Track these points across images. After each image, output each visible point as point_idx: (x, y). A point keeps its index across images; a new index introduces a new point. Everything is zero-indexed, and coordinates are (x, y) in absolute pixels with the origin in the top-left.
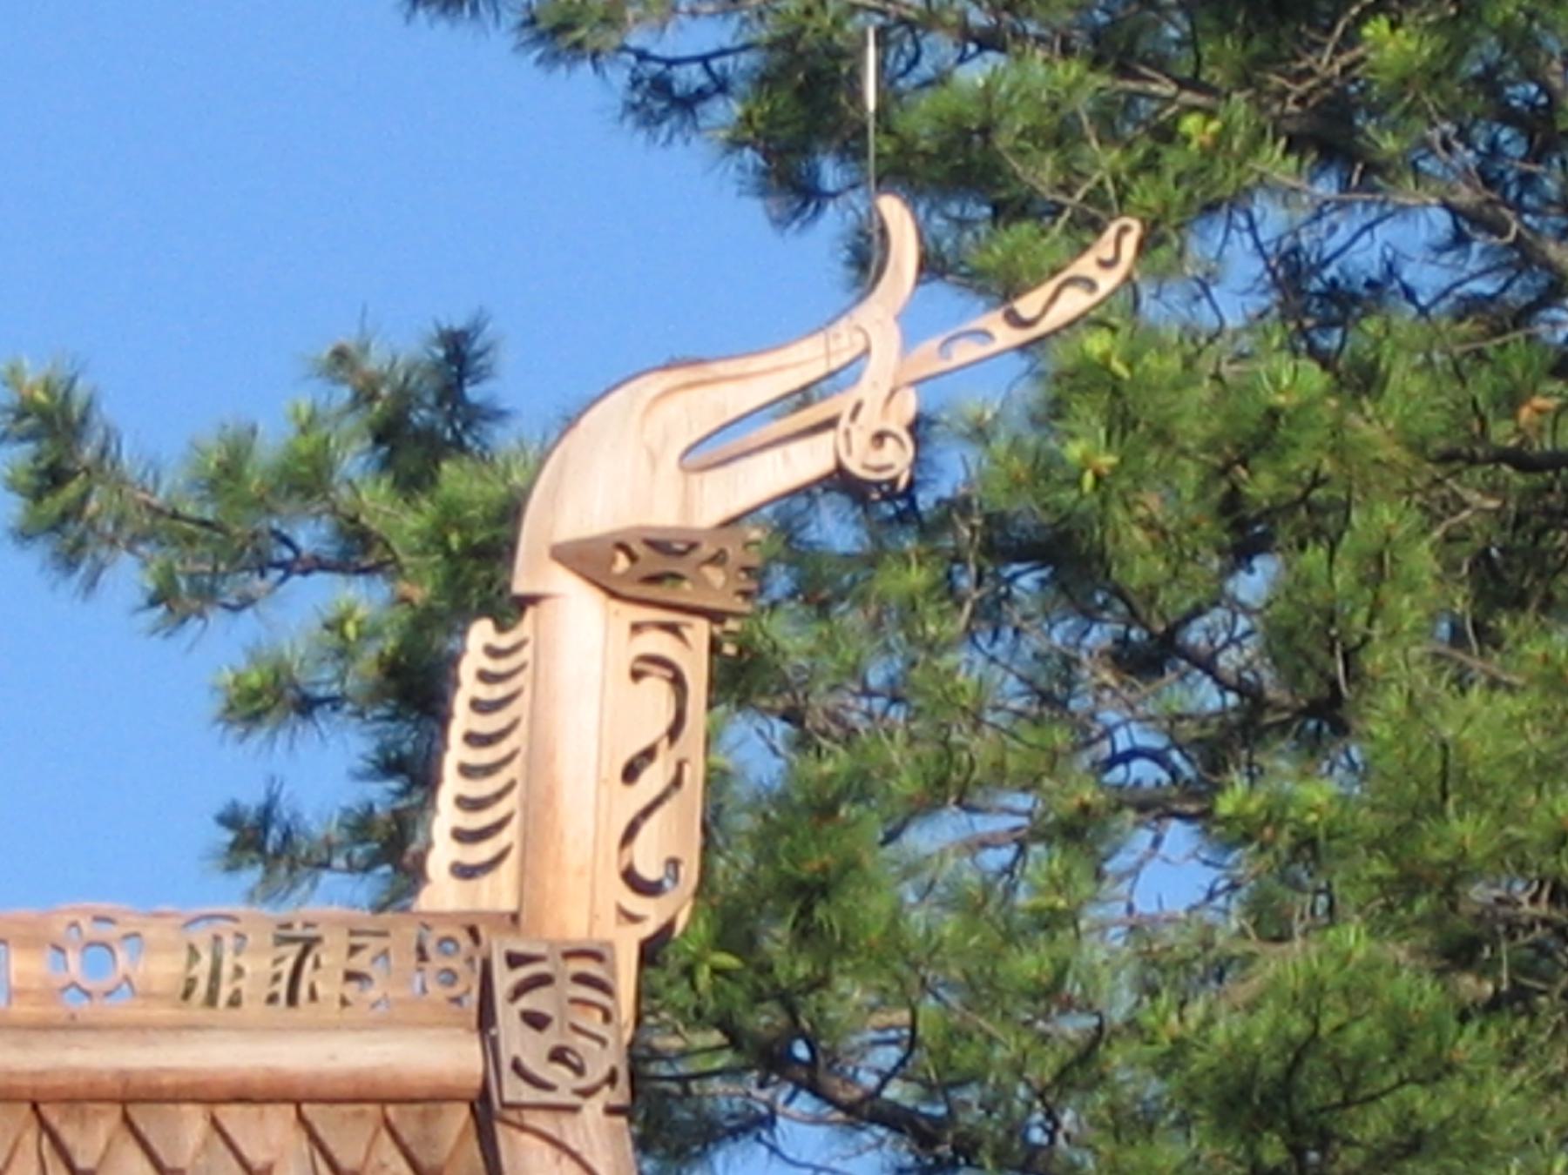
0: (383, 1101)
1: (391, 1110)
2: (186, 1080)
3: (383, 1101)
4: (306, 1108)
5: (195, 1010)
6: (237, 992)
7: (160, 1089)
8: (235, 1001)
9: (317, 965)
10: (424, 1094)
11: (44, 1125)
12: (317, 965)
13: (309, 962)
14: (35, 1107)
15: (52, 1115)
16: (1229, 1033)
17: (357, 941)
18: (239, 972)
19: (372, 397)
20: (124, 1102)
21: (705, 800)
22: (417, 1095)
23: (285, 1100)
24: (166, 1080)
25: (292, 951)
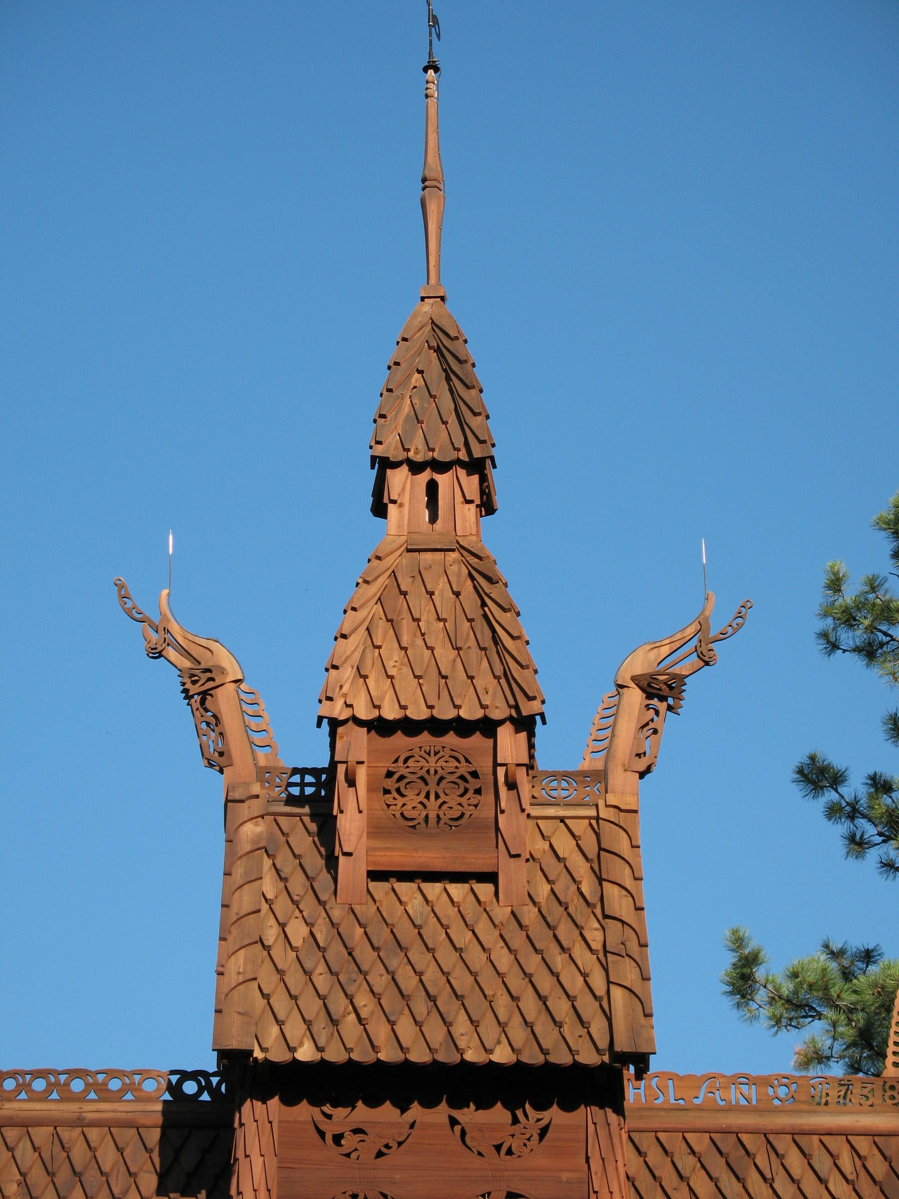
0: (873, 1135)
1: (876, 1138)
2: (812, 1127)
3: (873, 1135)
4: (848, 1137)
5: (823, 1108)
6: (827, 1101)
7: (803, 1130)
8: (826, 1104)
9: (852, 1093)
10: (886, 1133)
11: (769, 1142)
12: (852, 1093)
13: (849, 1092)
14: (765, 1135)
15: (771, 1137)
16: (628, 1070)
17: (864, 1085)
18: (827, 1094)
19: (893, 812)
20: (846, 1135)
21: (645, 925)
22: (883, 1133)
23: (708, 1132)
24: (806, 1128)
25: (844, 1088)
